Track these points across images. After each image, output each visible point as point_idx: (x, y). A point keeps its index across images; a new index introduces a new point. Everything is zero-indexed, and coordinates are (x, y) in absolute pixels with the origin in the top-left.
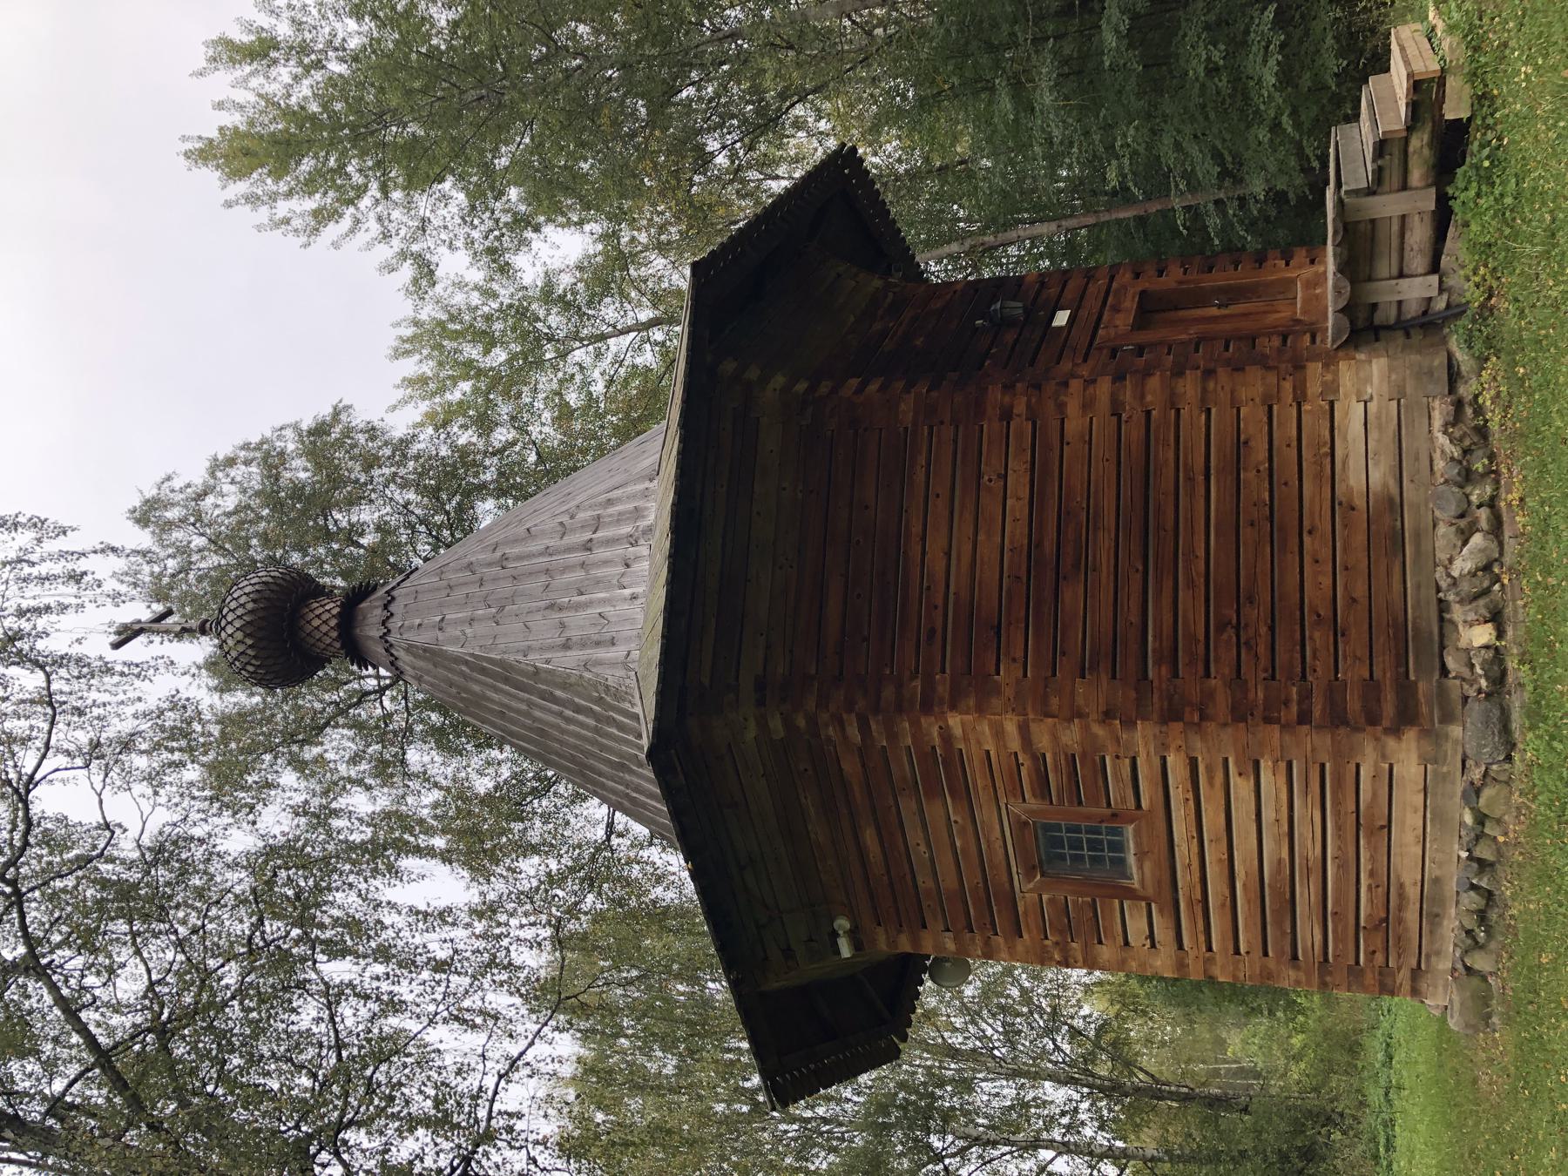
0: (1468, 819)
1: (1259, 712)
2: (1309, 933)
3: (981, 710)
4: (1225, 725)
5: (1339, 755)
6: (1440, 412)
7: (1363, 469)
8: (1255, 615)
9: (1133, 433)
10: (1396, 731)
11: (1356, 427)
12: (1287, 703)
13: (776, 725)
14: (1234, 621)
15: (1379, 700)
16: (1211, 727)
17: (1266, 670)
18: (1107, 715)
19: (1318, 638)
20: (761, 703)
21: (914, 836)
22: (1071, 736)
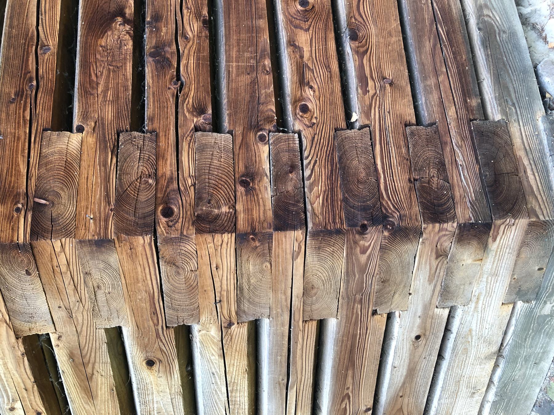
1: (183, 206)
4: (102, 244)
14: (130, 11)
15: (441, 166)
16: (61, 251)
17: (200, 110)
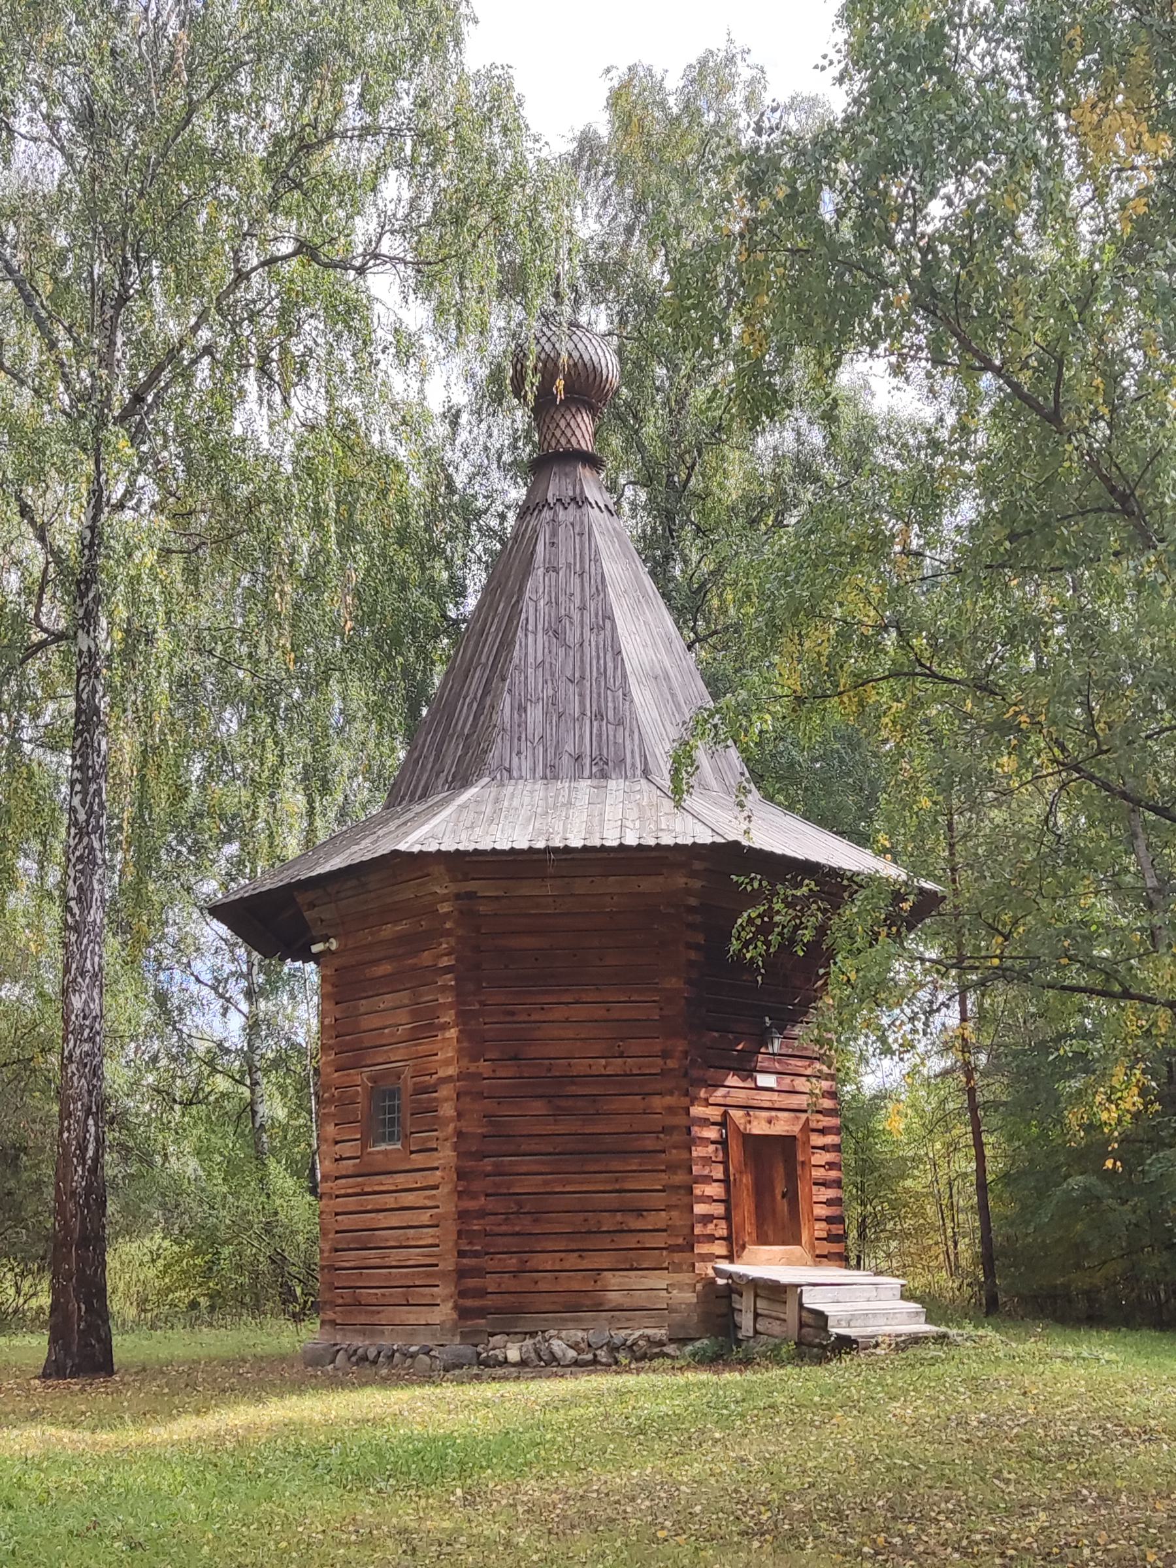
0: (413, 1349)
2: (351, 1258)
3: (460, 1051)
5: (444, 1274)
6: (660, 1333)
7: (619, 1286)
8: (525, 1224)
9: (649, 1143)
10: (456, 1307)
11: (649, 1283)
12: (470, 1243)
13: (444, 908)
18: (460, 1134)
19: (512, 1262)
20: (458, 896)
21: (388, 1000)
22: (447, 1110)
